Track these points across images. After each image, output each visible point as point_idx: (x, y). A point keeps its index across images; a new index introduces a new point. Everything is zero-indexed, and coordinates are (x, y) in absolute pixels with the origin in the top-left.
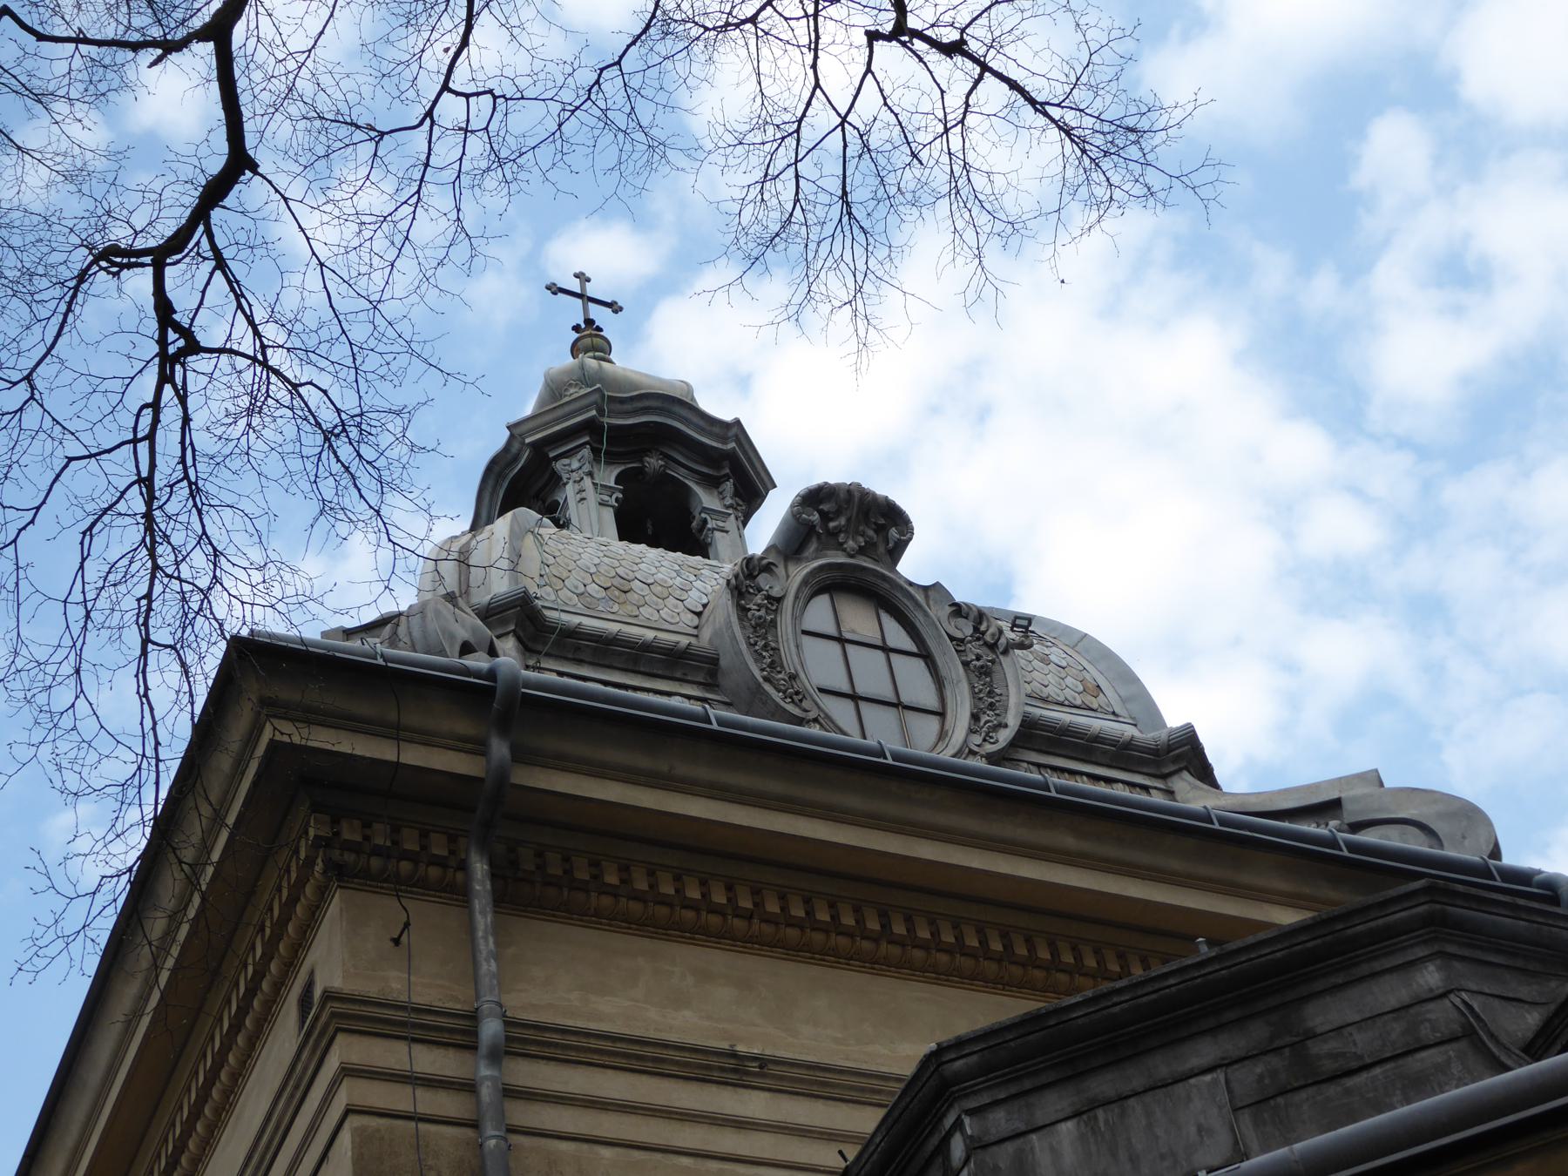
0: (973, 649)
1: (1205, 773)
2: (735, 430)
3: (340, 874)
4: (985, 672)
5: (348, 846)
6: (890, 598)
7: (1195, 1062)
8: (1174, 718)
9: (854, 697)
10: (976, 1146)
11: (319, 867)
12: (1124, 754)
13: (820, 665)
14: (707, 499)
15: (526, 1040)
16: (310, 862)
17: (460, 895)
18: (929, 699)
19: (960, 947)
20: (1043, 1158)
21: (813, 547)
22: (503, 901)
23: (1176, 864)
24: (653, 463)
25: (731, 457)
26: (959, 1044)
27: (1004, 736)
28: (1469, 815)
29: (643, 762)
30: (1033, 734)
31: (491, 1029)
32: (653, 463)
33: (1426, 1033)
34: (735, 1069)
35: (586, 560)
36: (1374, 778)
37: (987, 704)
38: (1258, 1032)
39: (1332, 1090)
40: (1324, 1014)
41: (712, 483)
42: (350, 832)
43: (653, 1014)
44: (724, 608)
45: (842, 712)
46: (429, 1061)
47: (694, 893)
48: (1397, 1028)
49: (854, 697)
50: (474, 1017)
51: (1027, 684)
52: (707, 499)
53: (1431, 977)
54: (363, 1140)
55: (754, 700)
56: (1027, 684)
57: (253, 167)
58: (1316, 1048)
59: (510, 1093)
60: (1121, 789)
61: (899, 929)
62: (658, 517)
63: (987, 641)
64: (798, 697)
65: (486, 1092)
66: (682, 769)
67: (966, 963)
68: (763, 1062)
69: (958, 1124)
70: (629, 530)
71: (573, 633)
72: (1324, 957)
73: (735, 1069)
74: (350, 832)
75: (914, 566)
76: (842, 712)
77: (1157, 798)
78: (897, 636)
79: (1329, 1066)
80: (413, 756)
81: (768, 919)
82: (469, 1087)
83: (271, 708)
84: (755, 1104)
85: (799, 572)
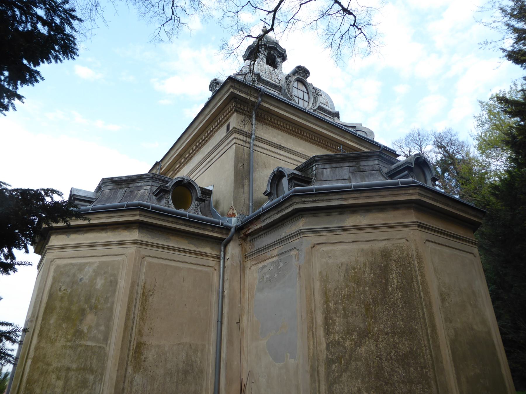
0: (314, 94)
1: (339, 118)
2: (284, 50)
3: (236, 111)
4: (315, 98)
5: (238, 108)
6: (305, 84)
7: (346, 165)
8: (337, 110)
9: (298, 98)
10: (317, 169)
11: (234, 110)
12: (329, 113)
13: (295, 92)
14: (279, 60)
15: (257, 139)
16: (233, 108)
17: (251, 118)
18: (307, 100)
19: (309, 137)
20: (325, 173)
21: (296, 75)
22: (257, 119)
23: (337, 133)
24: (272, 52)
25: (283, 54)
26: (318, 156)
27: (316, 107)
28: (372, 133)
29: (277, 105)
30: (320, 108)
31: (253, 136)
32: (272, 52)
33: (374, 169)
34: (280, 147)
35: (262, 67)
36: (361, 125)
37: (315, 102)
38: (354, 163)
39: (362, 173)
40: (363, 163)
41: (279, 57)
42: (238, 106)
43: (271, 138)
44: (284, 80)
45: (296, 99)
46: (244, 138)
47: (279, 123)
48: (371, 167)
49: (298, 98)
50: (251, 134)
51: (321, 101)
52: (279, 60)
53: (376, 162)
54: (236, 147)
55: (285, 95)
56: (321, 101)
57: (273, 30)
58: (361, 167)
59: (254, 145)
60: (327, 118)
61: (302, 133)
62: (272, 62)
63: (317, 93)
64: (291, 96)
65: (251, 145)
66: (281, 107)
67: (312, 141)
68: (284, 147)
69: (315, 166)
70: (268, 63)
71: (264, 80)
72: (365, 156)
73: (280, 147)
74: (238, 106)
75: (309, 80)
76: (296, 99)
77: (332, 120)
78: (305, 90)
79: (362, 170)
80: (241, 94)
81: (287, 128)
82: (250, 143)
83: (232, 87)
84: (282, 152)
85: (294, 78)
